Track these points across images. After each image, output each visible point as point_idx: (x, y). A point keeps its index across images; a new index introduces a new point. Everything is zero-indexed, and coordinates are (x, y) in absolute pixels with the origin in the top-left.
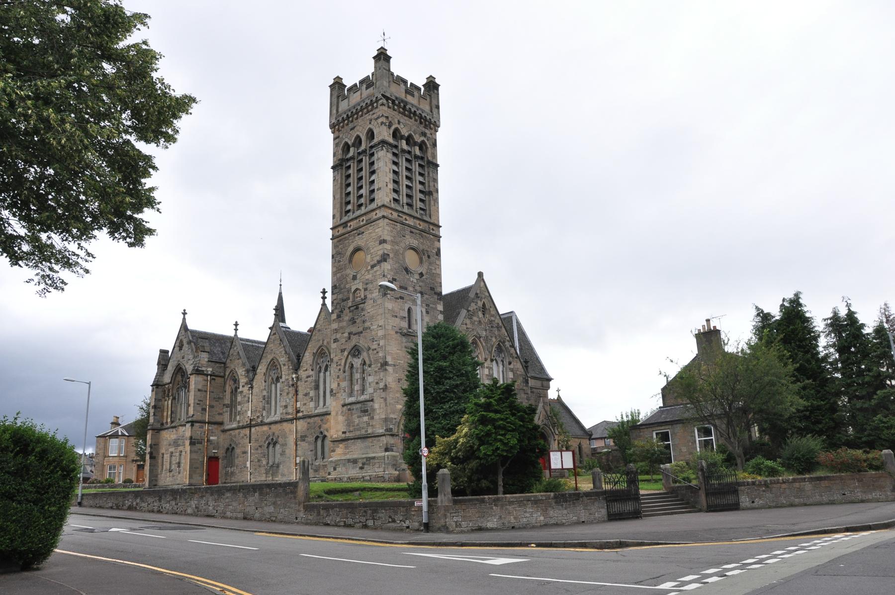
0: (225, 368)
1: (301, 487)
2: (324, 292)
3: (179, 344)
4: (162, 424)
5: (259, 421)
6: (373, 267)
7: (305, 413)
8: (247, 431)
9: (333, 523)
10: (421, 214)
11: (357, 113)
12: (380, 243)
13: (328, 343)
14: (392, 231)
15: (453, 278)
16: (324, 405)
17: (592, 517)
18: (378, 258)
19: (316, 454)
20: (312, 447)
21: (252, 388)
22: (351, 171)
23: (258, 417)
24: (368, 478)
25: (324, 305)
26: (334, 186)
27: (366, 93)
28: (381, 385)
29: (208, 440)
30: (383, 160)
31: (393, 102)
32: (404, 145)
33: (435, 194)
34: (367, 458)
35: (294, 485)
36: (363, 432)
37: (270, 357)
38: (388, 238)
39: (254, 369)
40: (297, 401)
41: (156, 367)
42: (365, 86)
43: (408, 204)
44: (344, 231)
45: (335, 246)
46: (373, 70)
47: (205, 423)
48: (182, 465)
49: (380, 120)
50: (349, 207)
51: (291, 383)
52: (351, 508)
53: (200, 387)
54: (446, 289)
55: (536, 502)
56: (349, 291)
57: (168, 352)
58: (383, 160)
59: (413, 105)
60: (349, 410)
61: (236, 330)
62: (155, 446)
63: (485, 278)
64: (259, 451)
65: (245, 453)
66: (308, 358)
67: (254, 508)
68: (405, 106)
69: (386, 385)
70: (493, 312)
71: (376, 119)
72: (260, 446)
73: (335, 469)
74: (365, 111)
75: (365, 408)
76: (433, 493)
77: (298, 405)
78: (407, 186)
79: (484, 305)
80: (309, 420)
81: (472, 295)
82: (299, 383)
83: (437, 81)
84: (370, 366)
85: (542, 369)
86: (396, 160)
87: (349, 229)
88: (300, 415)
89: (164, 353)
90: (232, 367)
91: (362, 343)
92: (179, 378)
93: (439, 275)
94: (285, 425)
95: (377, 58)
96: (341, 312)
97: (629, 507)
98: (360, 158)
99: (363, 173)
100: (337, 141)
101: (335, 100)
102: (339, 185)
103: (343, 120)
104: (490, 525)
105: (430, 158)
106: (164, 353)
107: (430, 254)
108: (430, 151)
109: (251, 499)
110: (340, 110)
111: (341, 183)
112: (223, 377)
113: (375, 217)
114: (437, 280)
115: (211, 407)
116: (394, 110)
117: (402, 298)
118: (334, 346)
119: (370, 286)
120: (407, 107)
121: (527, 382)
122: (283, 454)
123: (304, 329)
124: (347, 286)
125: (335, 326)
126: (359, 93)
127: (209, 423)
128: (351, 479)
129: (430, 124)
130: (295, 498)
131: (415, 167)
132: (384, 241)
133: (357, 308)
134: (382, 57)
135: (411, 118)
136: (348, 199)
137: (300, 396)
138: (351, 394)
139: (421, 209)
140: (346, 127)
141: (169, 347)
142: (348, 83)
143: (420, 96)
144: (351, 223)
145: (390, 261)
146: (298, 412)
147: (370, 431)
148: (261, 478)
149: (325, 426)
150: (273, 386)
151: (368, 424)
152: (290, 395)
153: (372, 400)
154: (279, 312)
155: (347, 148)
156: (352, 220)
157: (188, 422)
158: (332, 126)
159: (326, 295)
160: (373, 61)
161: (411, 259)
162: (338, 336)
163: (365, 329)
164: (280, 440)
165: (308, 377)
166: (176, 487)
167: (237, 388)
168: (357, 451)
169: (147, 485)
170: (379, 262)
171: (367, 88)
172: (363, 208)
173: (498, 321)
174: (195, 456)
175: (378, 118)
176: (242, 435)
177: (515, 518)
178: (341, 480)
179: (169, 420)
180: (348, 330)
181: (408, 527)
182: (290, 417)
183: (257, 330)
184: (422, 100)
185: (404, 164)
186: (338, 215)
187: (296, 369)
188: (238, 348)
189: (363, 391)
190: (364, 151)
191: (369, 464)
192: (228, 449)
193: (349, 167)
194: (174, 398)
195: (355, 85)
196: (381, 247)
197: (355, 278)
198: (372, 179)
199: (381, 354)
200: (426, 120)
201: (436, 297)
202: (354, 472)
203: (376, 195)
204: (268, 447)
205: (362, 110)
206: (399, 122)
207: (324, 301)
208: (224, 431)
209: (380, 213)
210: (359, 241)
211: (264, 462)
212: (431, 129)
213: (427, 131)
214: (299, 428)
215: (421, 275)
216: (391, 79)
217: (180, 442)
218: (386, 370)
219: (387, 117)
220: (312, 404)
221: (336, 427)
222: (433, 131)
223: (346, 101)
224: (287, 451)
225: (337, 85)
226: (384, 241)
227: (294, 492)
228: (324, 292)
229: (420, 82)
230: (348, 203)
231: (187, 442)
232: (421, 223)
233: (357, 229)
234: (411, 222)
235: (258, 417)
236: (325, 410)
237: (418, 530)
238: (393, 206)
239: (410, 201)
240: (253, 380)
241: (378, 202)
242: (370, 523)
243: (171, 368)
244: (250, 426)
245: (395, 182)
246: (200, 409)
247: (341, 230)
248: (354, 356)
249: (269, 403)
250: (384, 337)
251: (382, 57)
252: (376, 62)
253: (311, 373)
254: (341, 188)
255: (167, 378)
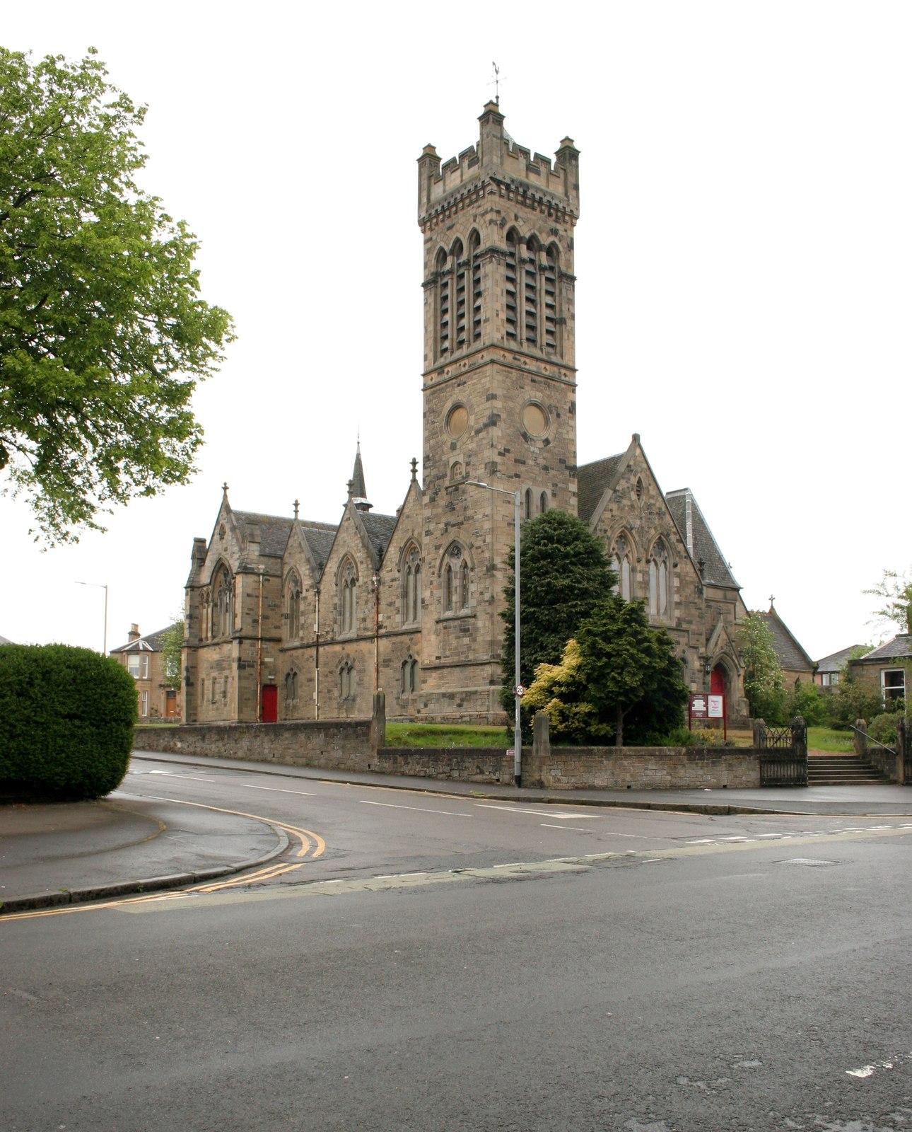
0: (283, 564)
1: (375, 727)
2: (414, 463)
3: (220, 531)
4: (201, 640)
5: (329, 638)
6: (478, 432)
7: (389, 629)
8: (313, 651)
9: (412, 773)
10: (548, 354)
11: (456, 204)
12: (488, 400)
13: (420, 534)
14: (504, 382)
15: (594, 442)
16: (415, 618)
17: (737, 781)
18: (485, 420)
19: (403, 685)
20: (398, 676)
21: (318, 592)
22: (448, 292)
23: (327, 633)
24: (468, 719)
25: (414, 480)
26: (426, 312)
27: (469, 173)
28: (487, 596)
29: (262, 663)
30: (493, 276)
31: (508, 187)
32: (524, 252)
33: (569, 322)
34: (466, 692)
35: (366, 724)
36: (462, 658)
37: (342, 552)
38: (499, 392)
39: (321, 567)
40: (378, 613)
41: (190, 561)
42: (466, 163)
43: (528, 340)
44: (440, 379)
45: (427, 401)
46: (478, 138)
47: (258, 639)
48: (229, 695)
49: (488, 217)
50: (447, 344)
51: (370, 587)
52: (434, 754)
53: (250, 591)
54: (582, 460)
55: (662, 757)
56: (445, 465)
57: (204, 541)
58: (493, 276)
59: (537, 189)
60: (445, 628)
61: (296, 512)
62: (192, 669)
63: (642, 442)
64: (330, 679)
65: (311, 680)
66: (393, 554)
67: (319, 752)
68: (525, 192)
69: (493, 597)
70: (653, 492)
71: (483, 215)
72: (331, 672)
73: (426, 706)
74: (467, 201)
75: (465, 627)
76: (527, 736)
77: (380, 619)
78: (528, 313)
79: (639, 481)
80: (394, 639)
81: (622, 468)
82: (381, 588)
83: (577, 146)
84: (472, 570)
85: (725, 573)
86: (511, 275)
87: (446, 376)
88: (382, 631)
89: (199, 542)
90: (292, 563)
91: (464, 538)
92: (221, 577)
93: (573, 442)
94: (364, 646)
95: (484, 119)
96: (436, 493)
97: (791, 771)
98: (461, 271)
99: (465, 295)
100: (429, 245)
101: (425, 182)
102: (432, 310)
103: (437, 214)
104: (597, 782)
105: (563, 269)
106: (199, 542)
107: (561, 412)
108: (563, 257)
109: (315, 741)
110: (433, 198)
111: (435, 309)
112: (280, 577)
113: (481, 361)
114: (571, 448)
115: (265, 617)
116: (509, 199)
117: (517, 476)
118: (426, 540)
119: (473, 460)
120: (529, 193)
121: (700, 592)
122: (360, 683)
123: (392, 512)
124: (444, 458)
125: (427, 512)
126: (458, 173)
127: (262, 639)
128: (445, 720)
129: (565, 214)
130: (368, 741)
131: (541, 284)
132: (493, 397)
133: (457, 489)
134: (491, 117)
135: (534, 209)
136: (444, 333)
137: (383, 606)
138: (448, 605)
139: (548, 345)
140: (441, 225)
141: (207, 535)
142: (446, 153)
143: (550, 173)
144: (450, 368)
145: (501, 424)
146: (380, 627)
147: (471, 657)
148: (331, 714)
149: (415, 648)
150: (348, 591)
151: (469, 648)
152: (370, 605)
153: (475, 616)
154: (357, 486)
155: (442, 256)
156: (451, 363)
157: (235, 638)
158: (422, 223)
159: (417, 467)
160: (478, 124)
161: (532, 420)
162: (432, 526)
163: (468, 519)
164: (357, 664)
165: (393, 580)
166: (221, 723)
167: (298, 593)
168: (454, 682)
169: (184, 720)
170: (486, 426)
171: (470, 166)
172: (465, 346)
173: (659, 504)
174: (245, 683)
175: (486, 213)
176: (306, 656)
177: (632, 776)
178: (432, 720)
179: (210, 635)
180: (444, 520)
181: (498, 780)
182: (369, 633)
183: (327, 508)
184: (552, 179)
185: (524, 280)
186: (431, 356)
187: (378, 569)
188: (297, 539)
189: (464, 601)
190: (467, 263)
191: (468, 701)
192: (288, 675)
193: (445, 285)
194: (215, 605)
195: (454, 160)
196: (488, 404)
197: (453, 447)
198: (478, 303)
199: (487, 555)
200: (557, 210)
201: (567, 472)
202: (449, 710)
203: (483, 329)
204: (340, 674)
205: (462, 200)
206: (516, 218)
207: (414, 476)
208: (283, 650)
209: (487, 356)
210: (457, 395)
211: (336, 693)
212: (565, 221)
213: (559, 227)
214: (381, 649)
215: (547, 442)
216: (504, 152)
217: (225, 665)
218: (493, 576)
219: (498, 212)
220: (398, 618)
221: (428, 649)
222: (568, 226)
223: (441, 183)
224: (366, 679)
225: (429, 158)
226: (493, 397)
227: (366, 734)
228: (414, 463)
229: (549, 150)
230: (445, 337)
231: (235, 665)
232: (548, 367)
233: (456, 377)
234: (532, 366)
235: (327, 633)
236: (415, 626)
237: (508, 785)
238: (506, 344)
239: (531, 335)
240: (319, 582)
241: (485, 340)
242: (455, 774)
243: (209, 564)
244: (317, 645)
245: (510, 308)
246: (250, 621)
247: (436, 378)
248: (452, 555)
249: (342, 613)
250: (492, 530)
251: (491, 117)
252: (482, 126)
253: (397, 575)
254: (435, 317)
255: (205, 577)
